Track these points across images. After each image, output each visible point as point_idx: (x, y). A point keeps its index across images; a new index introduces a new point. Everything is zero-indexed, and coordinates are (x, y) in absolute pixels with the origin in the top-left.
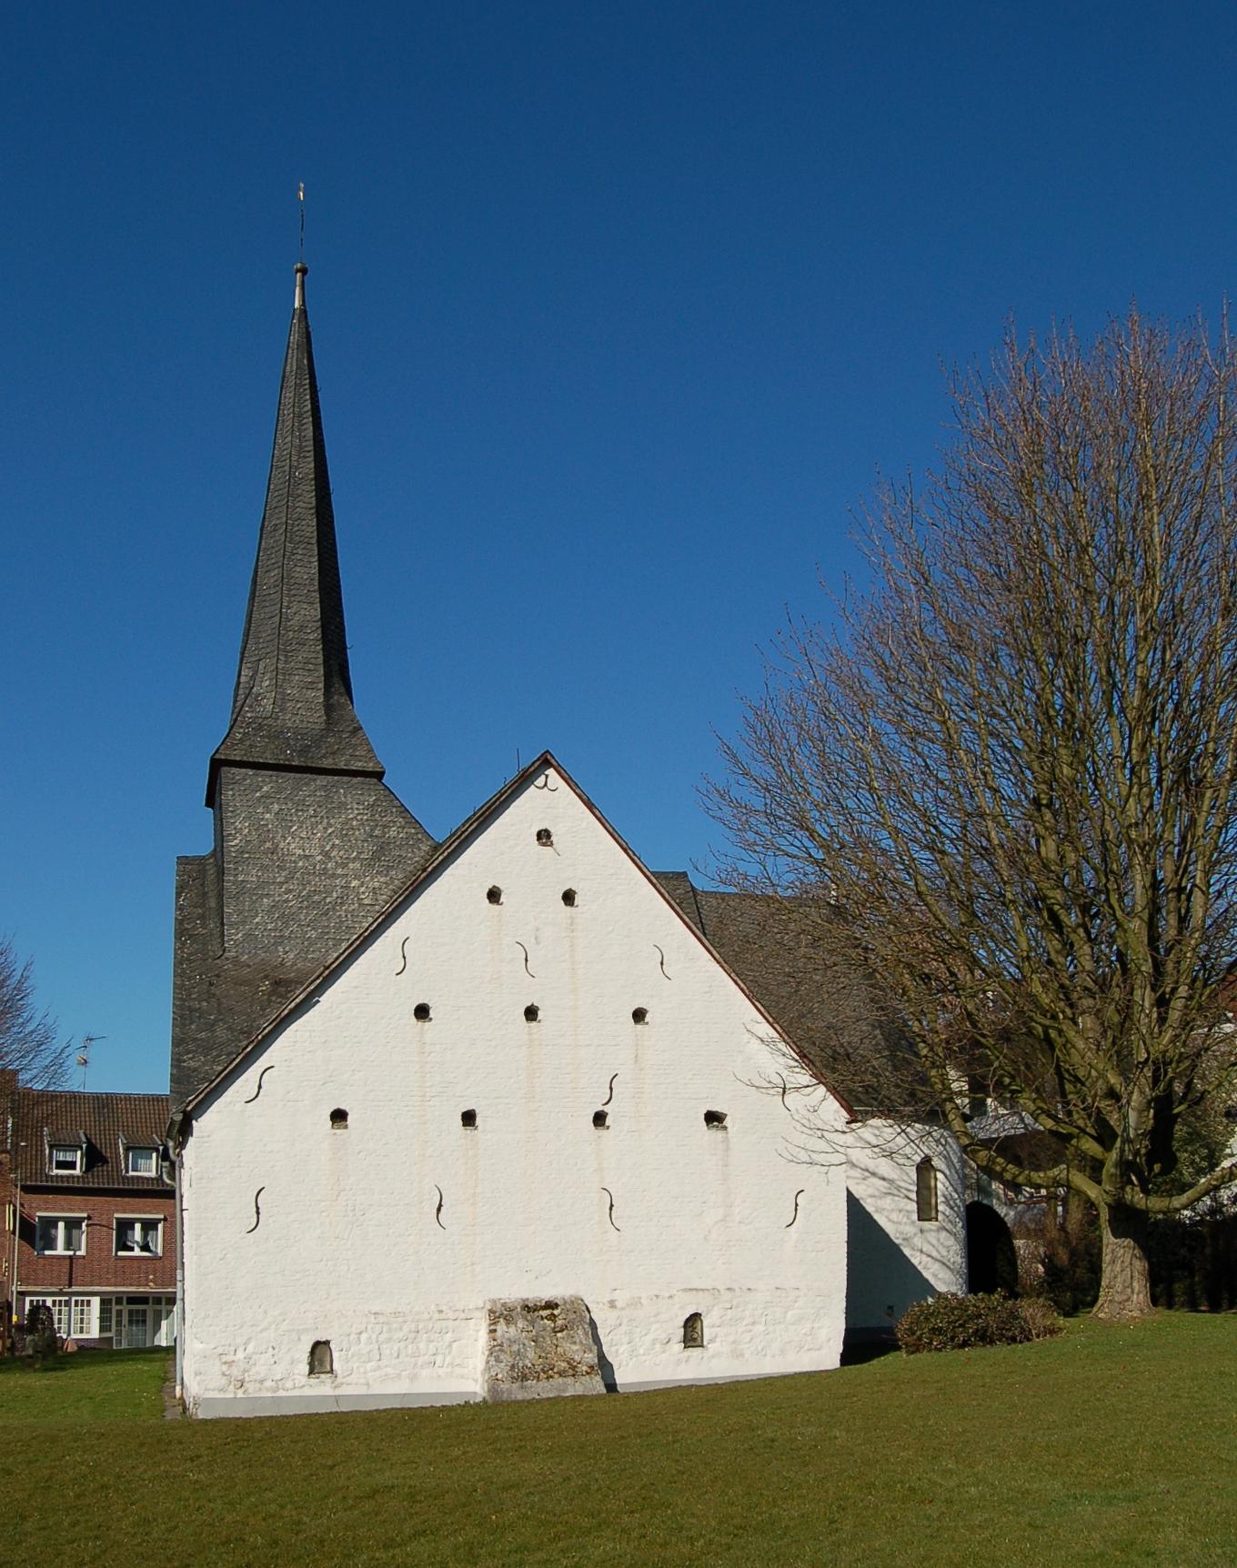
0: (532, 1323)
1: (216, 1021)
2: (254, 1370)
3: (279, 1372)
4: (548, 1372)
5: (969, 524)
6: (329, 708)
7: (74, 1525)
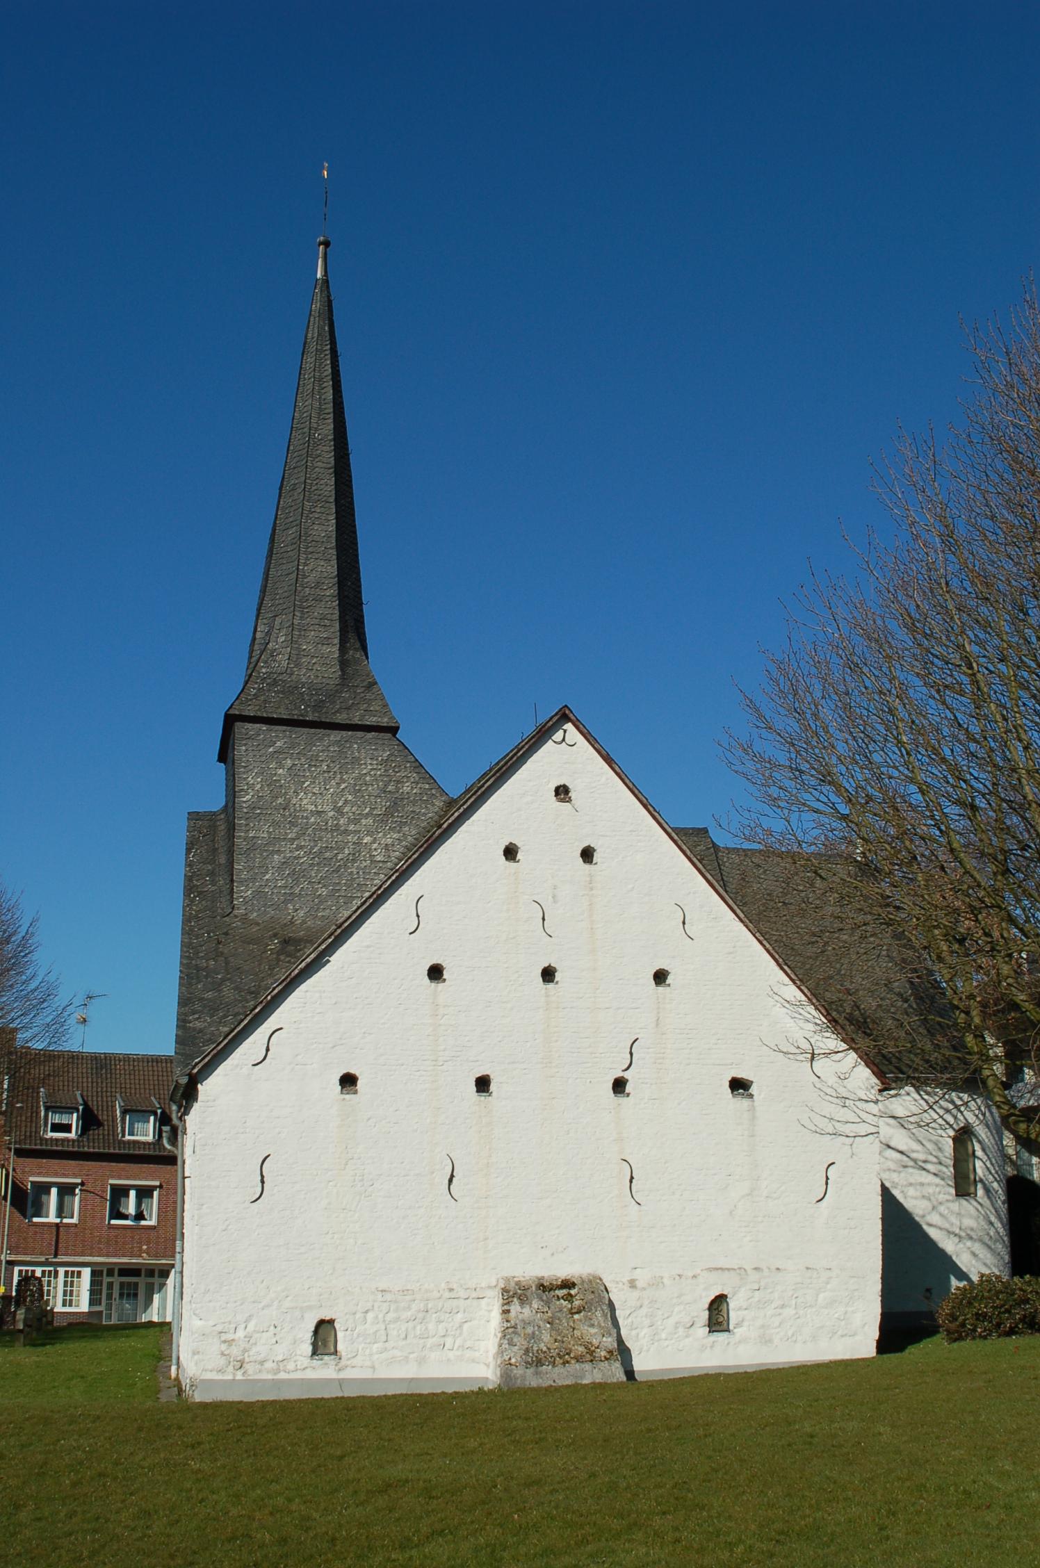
0: (548, 1303)
1: (223, 980)
2: (254, 1350)
3: (280, 1352)
4: (564, 1357)
5: (993, 476)
6: (344, 663)
7: (71, 1515)
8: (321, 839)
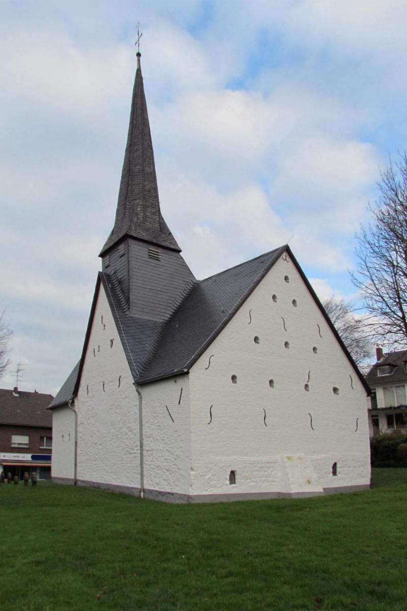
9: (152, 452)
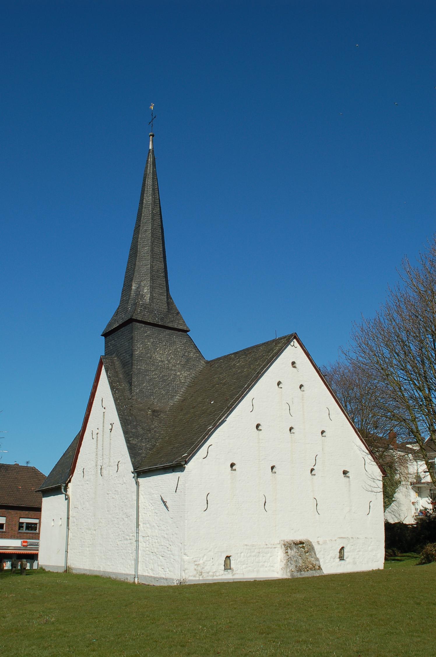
0: (298, 549)
4: (307, 568)
8: (163, 371)
9: (148, 538)
